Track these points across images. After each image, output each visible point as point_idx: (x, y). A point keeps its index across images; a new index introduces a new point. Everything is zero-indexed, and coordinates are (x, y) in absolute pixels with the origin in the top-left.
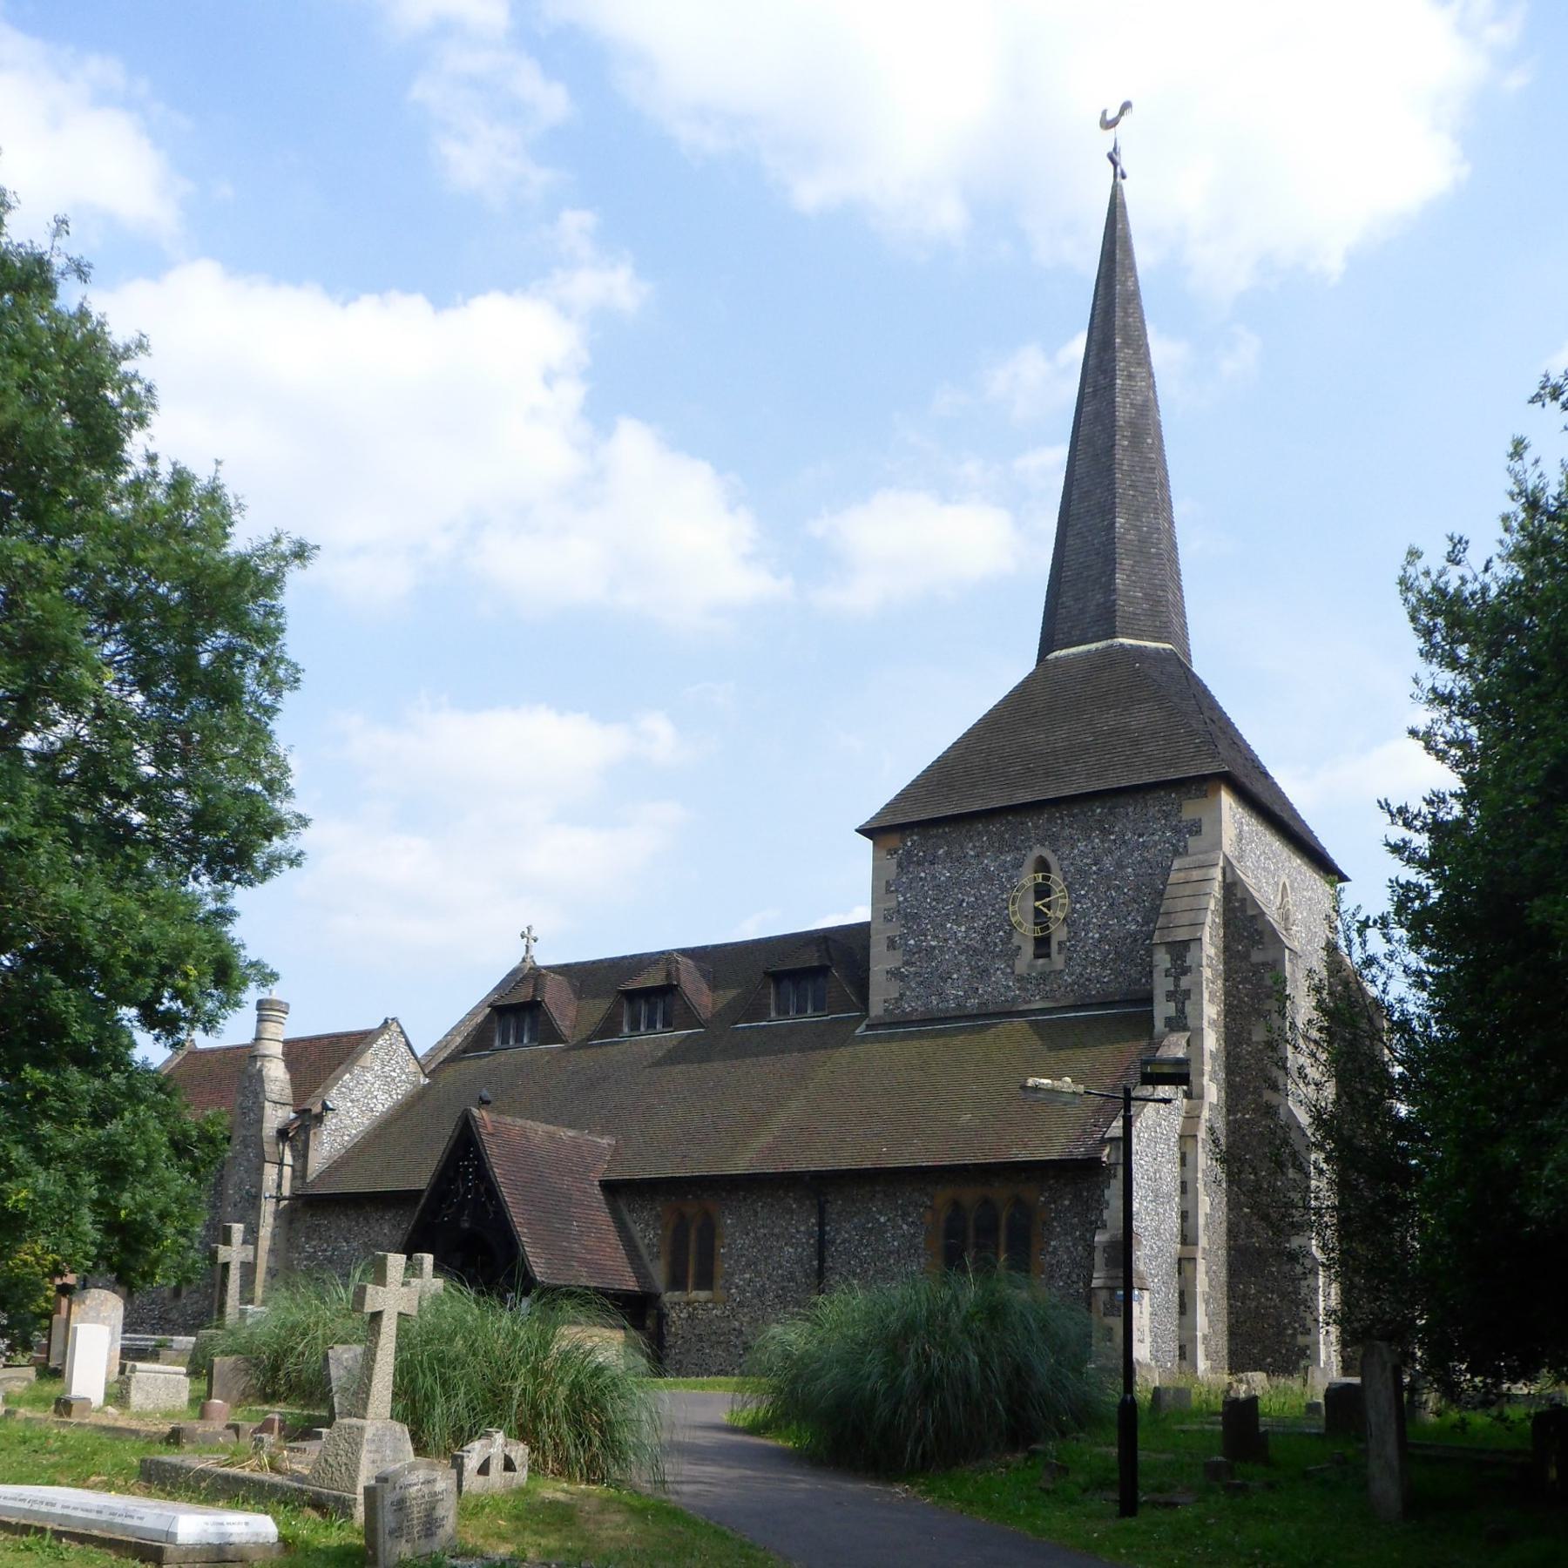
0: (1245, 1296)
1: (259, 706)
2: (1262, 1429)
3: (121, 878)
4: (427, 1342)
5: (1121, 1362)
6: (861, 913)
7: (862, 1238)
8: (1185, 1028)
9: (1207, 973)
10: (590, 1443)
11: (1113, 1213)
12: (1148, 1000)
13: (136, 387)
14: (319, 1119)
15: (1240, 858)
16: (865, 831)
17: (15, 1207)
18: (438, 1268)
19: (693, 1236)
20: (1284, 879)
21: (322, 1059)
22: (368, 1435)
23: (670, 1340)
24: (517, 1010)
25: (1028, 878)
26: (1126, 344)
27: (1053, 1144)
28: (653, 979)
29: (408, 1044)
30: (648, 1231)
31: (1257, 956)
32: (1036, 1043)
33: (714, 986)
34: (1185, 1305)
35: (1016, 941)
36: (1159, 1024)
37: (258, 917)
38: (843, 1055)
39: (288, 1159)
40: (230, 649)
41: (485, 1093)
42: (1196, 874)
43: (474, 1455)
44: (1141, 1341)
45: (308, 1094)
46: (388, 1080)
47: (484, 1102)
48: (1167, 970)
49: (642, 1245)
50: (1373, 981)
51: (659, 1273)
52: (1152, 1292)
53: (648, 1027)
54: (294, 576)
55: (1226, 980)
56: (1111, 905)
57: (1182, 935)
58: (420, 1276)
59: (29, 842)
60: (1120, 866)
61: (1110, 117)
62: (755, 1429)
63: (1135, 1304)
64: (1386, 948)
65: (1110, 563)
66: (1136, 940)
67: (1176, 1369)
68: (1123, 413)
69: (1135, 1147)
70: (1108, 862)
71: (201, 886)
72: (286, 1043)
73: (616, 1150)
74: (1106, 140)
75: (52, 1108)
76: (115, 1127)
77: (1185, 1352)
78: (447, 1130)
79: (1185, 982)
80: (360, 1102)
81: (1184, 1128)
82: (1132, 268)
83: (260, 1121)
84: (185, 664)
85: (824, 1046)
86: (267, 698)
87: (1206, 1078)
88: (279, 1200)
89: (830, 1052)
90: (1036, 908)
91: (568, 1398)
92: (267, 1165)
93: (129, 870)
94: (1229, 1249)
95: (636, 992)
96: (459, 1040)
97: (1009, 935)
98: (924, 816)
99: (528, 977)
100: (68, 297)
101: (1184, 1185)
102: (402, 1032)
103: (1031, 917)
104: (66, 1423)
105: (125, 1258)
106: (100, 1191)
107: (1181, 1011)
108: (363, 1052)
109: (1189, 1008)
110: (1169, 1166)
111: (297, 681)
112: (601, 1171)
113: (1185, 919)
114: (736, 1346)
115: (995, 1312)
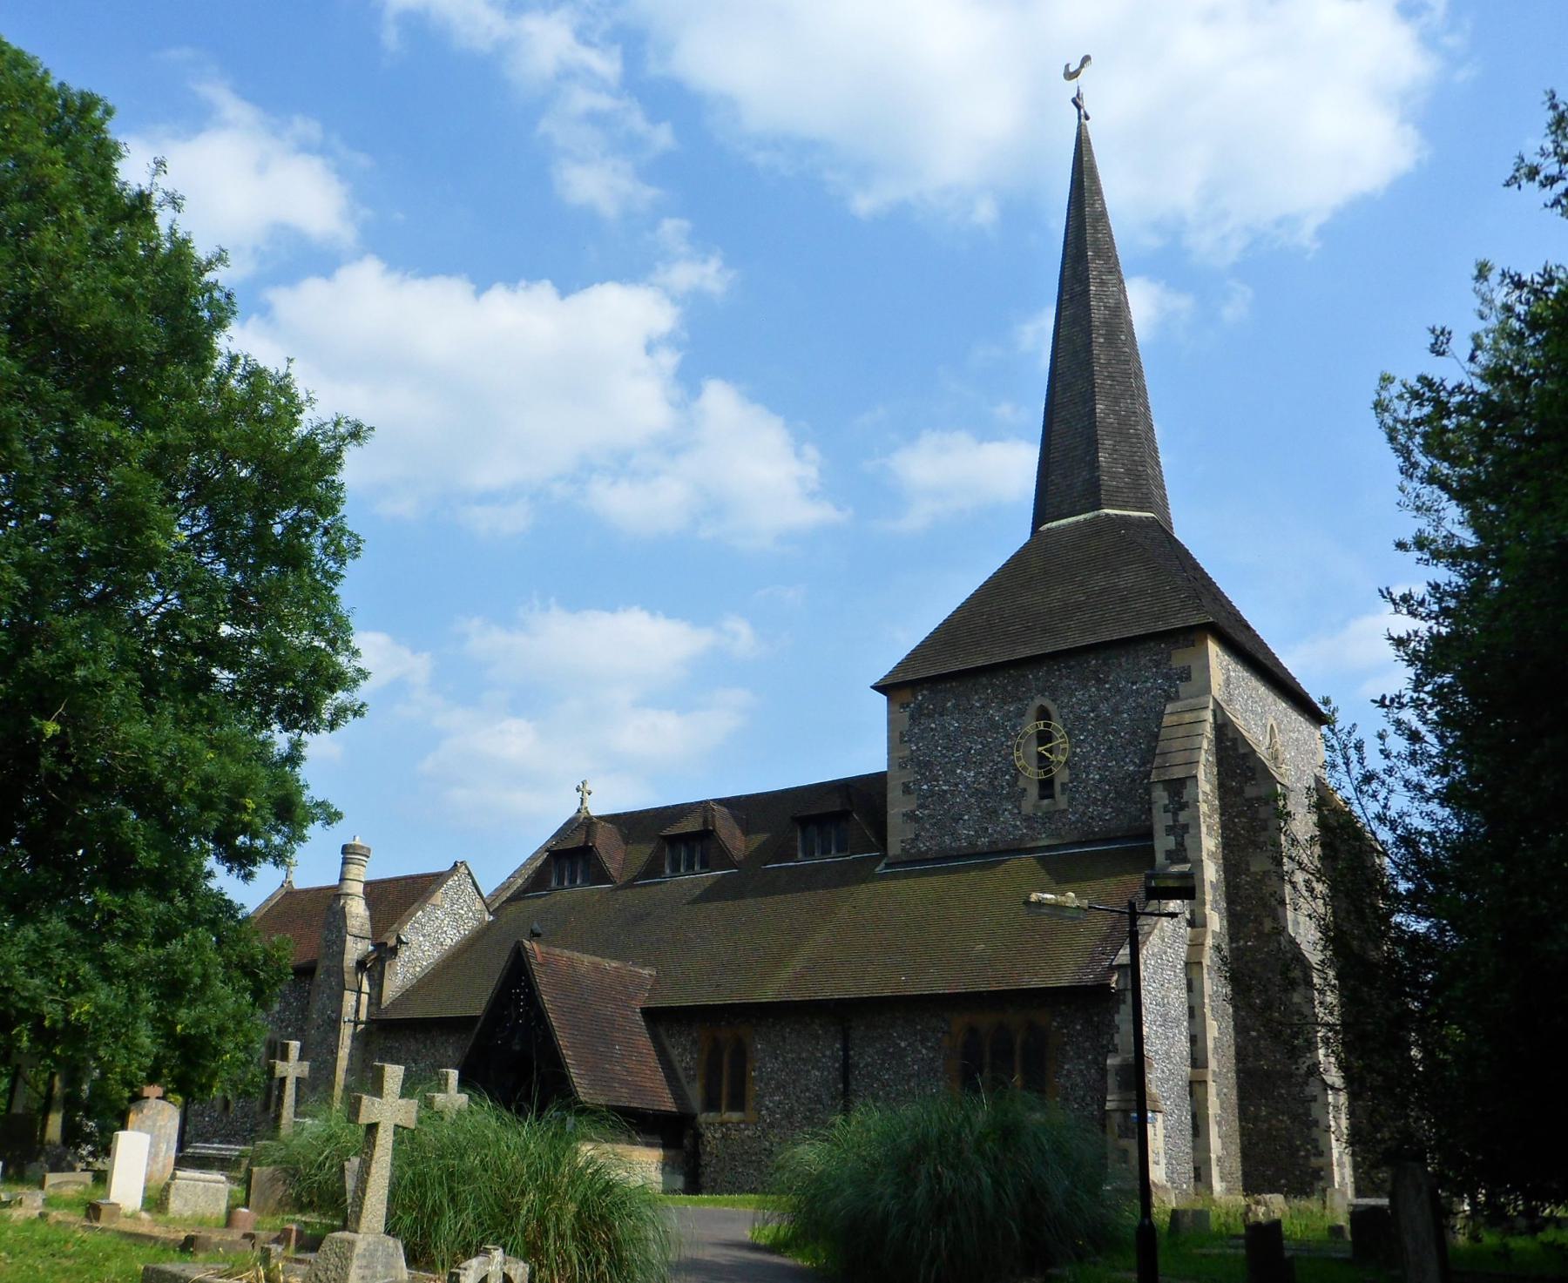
0: (1256, 1118)
1: (325, 573)
2: (1287, 1254)
3: (193, 722)
4: (441, 1157)
5: (1137, 1185)
6: (881, 766)
7: (884, 1062)
9: (1204, 808)
10: (598, 1262)
11: (1124, 1037)
12: (1148, 835)
13: (216, 294)
14: (394, 952)
15: (1230, 701)
16: (878, 688)
17: (77, 1019)
18: (463, 1084)
19: (726, 1058)
20: (1271, 721)
21: (398, 898)
22: (360, 1247)
23: (705, 1159)
24: (573, 854)
25: (1031, 726)
26: (1097, 255)
27: (1064, 970)
28: (691, 825)
29: (474, 884)
30: (685, 1057)
31: (1250, 791)
32: (1043, 874)
33: (747, 831)
34: (1198, 1128)
35: (1021, 783)
37: (323, 760)
38: (863, 892)
39: (366, 987)
40: (298, 522)
41: (536, 926)
42: (1188, 717)
43: (471, 1272)
44: (1157, 1163)
45: (386, 930)
46: (457, 918)
47: (534, 935)
48: (1166, 806)
49: (679, 1067)
50: (1374, 796)
51: (695, 1094)
52: (1165, 1115)
54: (350, 454)
55: (1222, 815)
56: (1110, 748)
57: (1178, 773)
58: (445, 1091)
59: (103, 685)
60: (1116, 711)
61: (1072, 69)
62: (774, 1248)
63: (1149, 1126)
64: (1385, 764)
65: (1092, 444)
66: (1133, 780)
67: (1191, 1190)
68: (1098, 314)
69: (1143, 974)
70: (1104, 708)
71: (280, 739)
72: (367, 884)
73: (657, 980)
74: (1070, 88)
75: (119, 929)
76: (175, 946)
77: (1200, 1174)
78: (499, 962)
79: (1183, 817)
80: (430, 938)
81: (1189, 955)
82: (1099, 192)
83: (342, 953)
84: (260, 534)
85: (847, 884)
86: (332, 565)
87: (1208, 907)
88: (356, 1025)
89: (852, 889)
90: (1040, 754)
91: (578, 1215)
92: (347, 993)
93: (200, 714)
94: (1238, 1072)
95: (674, 838)
96: (520, 881)
97: (1015, 778)
98: (933, 673)
99: (582, 825)
100: (163, 219)
101: (1191, 1010)
102: (469, 874)
103: (1034, 761)
104: (93, 1228)
105: (186, 1068)
106: (160, 1007)
107: (1181, 845)
108: (434, 892)
109: (1188, 841)
110: (1175, 977)
111: (358, 549)
112: (642, 1000)
113: (1180, 758)
115: (1008, 1133)
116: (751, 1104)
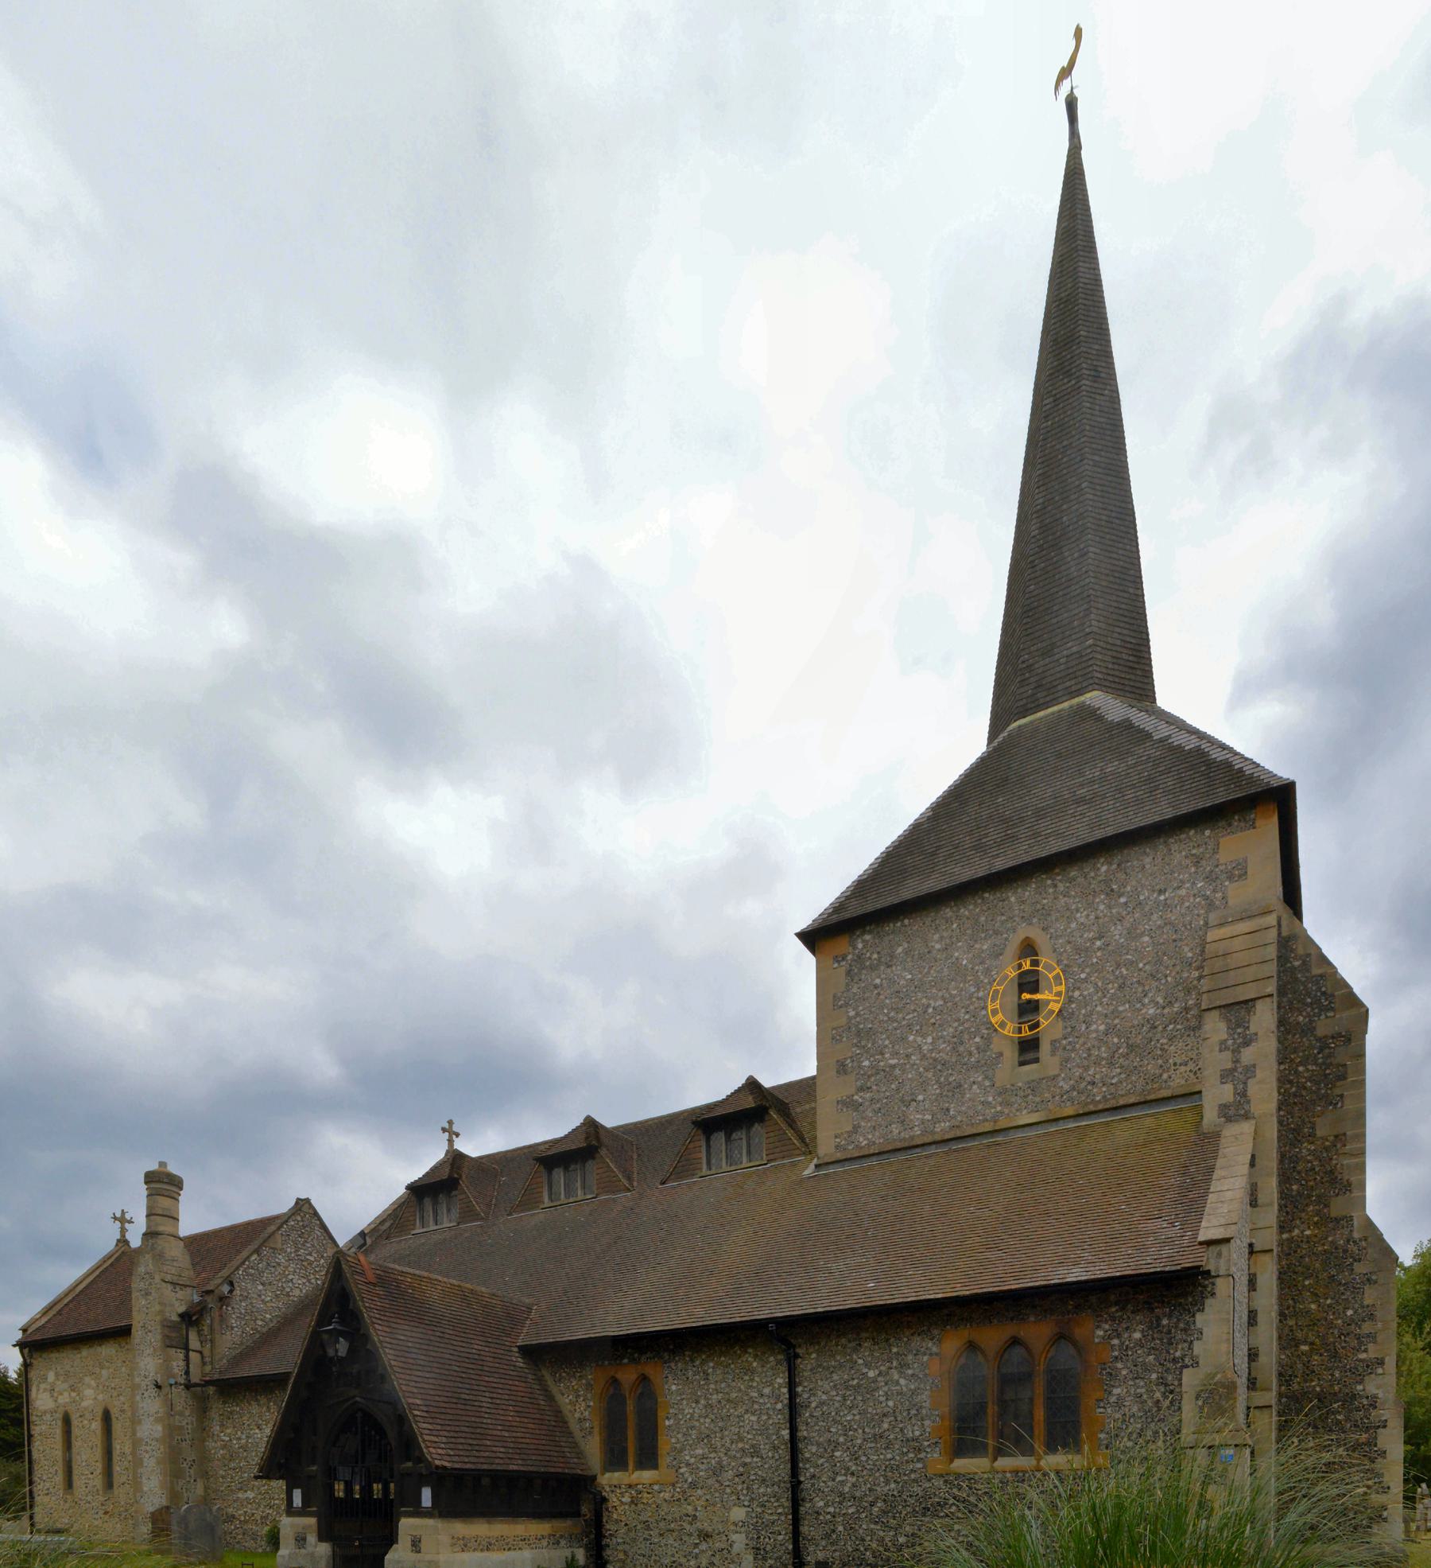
8: (1247, 1117)
23: (610, 1527)
31: (1324, 1027)
36: (1210, 1116)
48: (1223, 1042)
51: (593, 1449)
53: (567, 1196)
60: (1132, 934)
70: (1117, 932)
97: (987, 1040)
107: (1242, 1094)
114: (690, 1535)
116: (664, 1460)
